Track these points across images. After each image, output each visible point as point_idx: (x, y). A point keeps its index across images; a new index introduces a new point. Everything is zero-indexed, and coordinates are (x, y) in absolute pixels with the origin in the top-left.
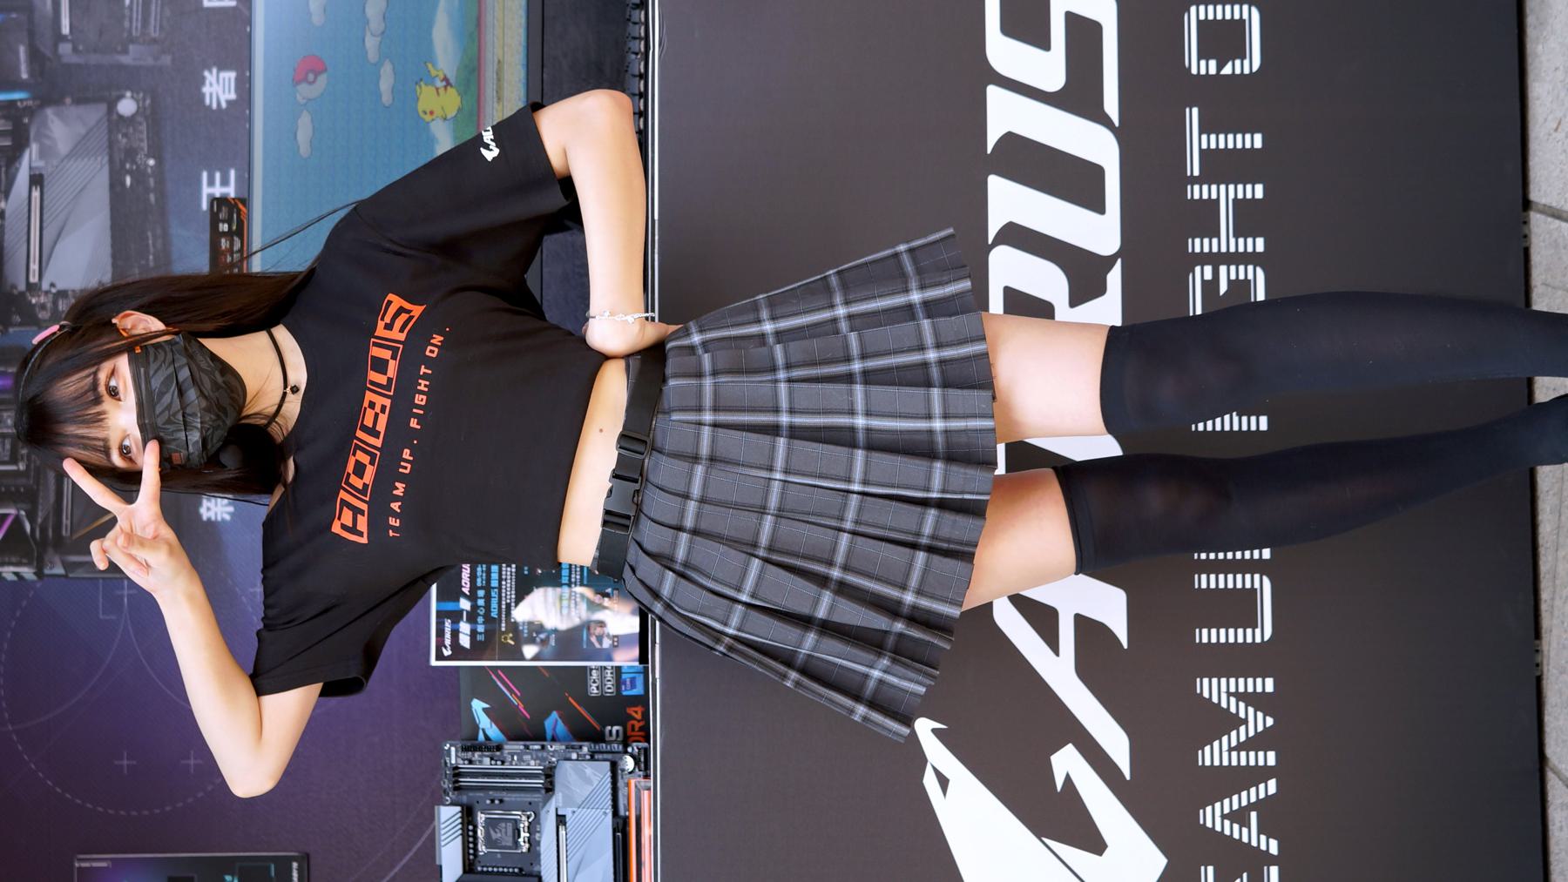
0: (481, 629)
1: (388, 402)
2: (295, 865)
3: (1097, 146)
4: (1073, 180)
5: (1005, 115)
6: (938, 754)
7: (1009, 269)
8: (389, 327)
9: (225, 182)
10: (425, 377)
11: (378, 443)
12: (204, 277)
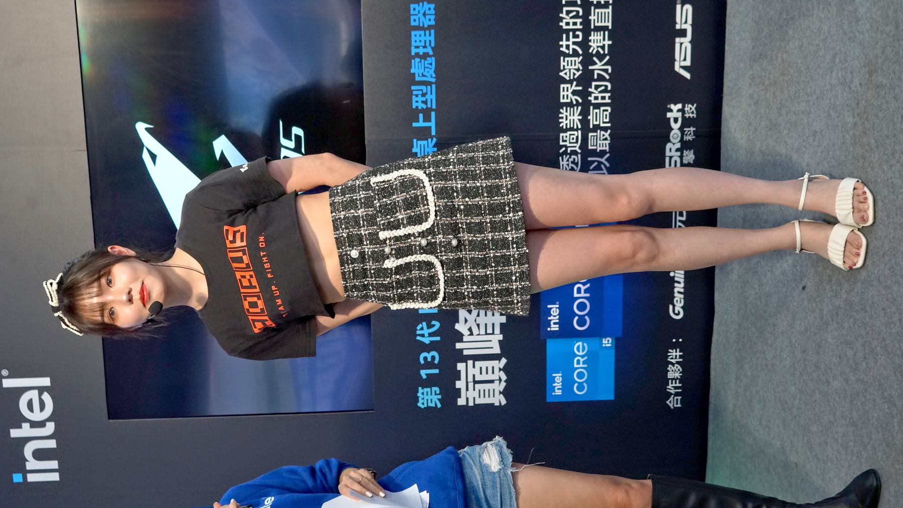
1: (252, 273)
2: (555, 328)
6: (149, 142)
8: (234, 241)
9: (425, 358)
10: (264, 256)
11: (258, 290)
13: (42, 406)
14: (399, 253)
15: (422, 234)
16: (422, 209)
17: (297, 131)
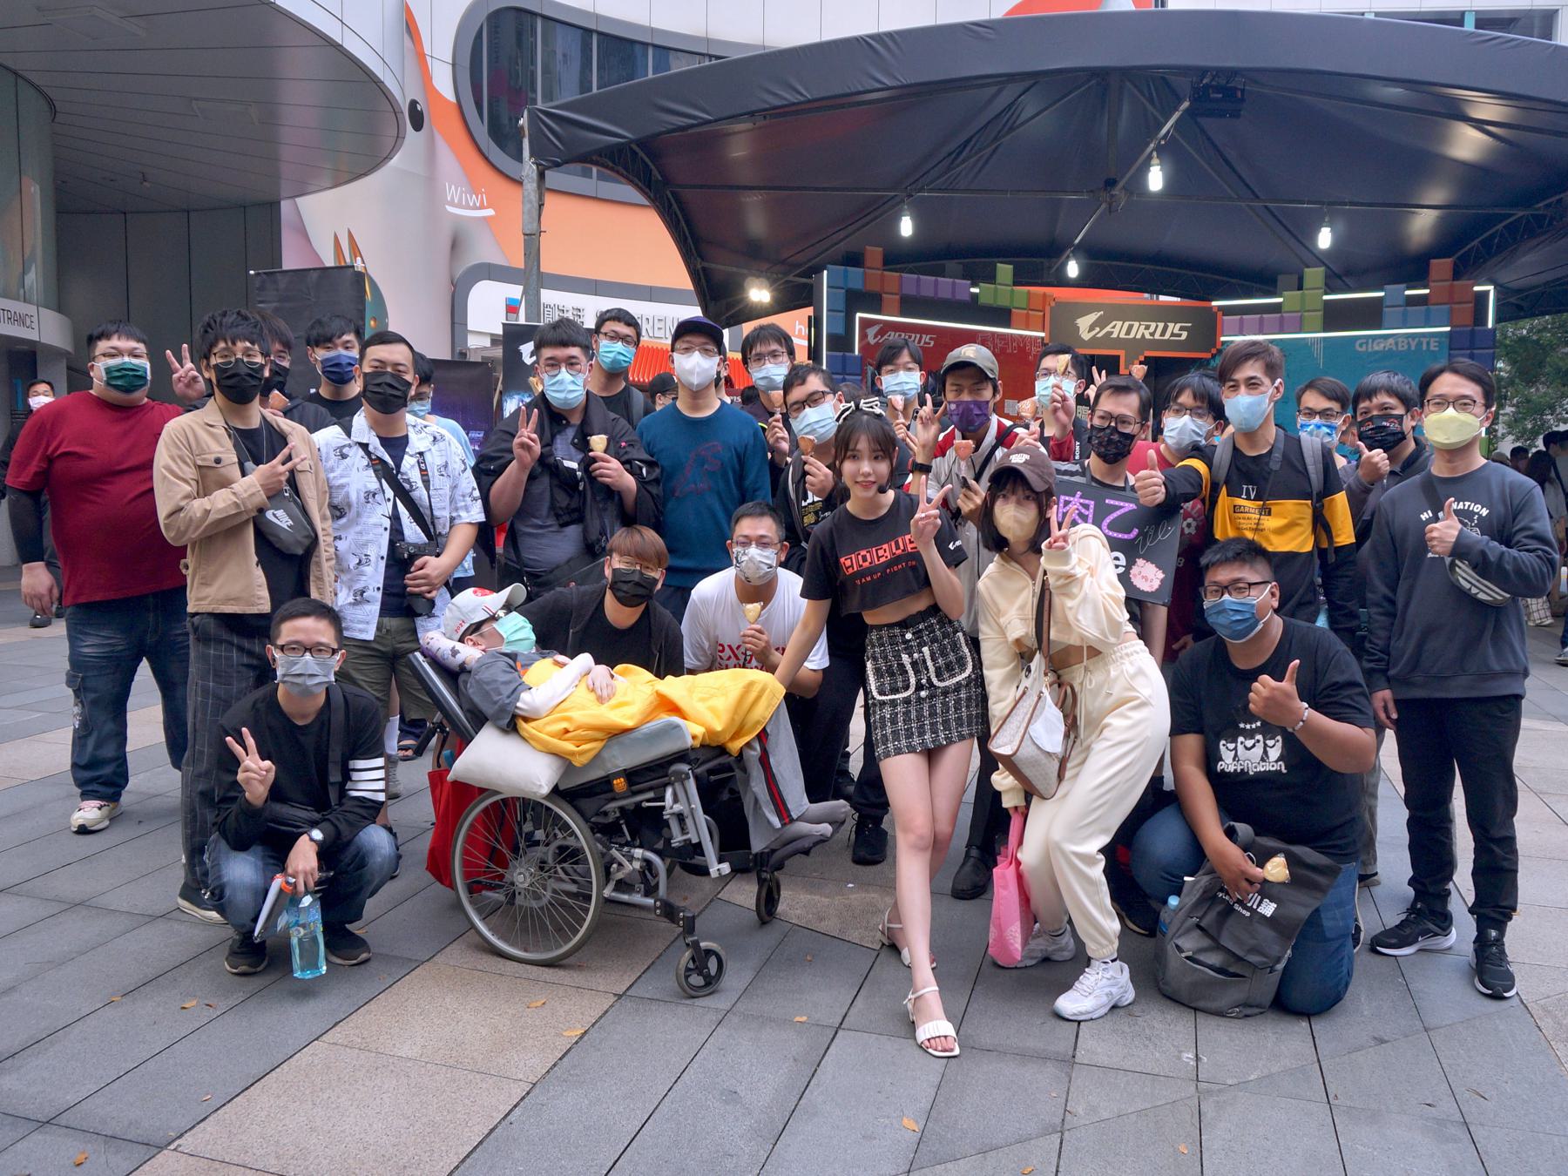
0: (905, 658)
3: (1167, 336)
4: (1163, 334)
5: (1171, 325)
7: (1153, 325)
12: (757, 281)
14: (914, 664)
15: (929, 680)
16: (946, 675)
17: (1185, 335)
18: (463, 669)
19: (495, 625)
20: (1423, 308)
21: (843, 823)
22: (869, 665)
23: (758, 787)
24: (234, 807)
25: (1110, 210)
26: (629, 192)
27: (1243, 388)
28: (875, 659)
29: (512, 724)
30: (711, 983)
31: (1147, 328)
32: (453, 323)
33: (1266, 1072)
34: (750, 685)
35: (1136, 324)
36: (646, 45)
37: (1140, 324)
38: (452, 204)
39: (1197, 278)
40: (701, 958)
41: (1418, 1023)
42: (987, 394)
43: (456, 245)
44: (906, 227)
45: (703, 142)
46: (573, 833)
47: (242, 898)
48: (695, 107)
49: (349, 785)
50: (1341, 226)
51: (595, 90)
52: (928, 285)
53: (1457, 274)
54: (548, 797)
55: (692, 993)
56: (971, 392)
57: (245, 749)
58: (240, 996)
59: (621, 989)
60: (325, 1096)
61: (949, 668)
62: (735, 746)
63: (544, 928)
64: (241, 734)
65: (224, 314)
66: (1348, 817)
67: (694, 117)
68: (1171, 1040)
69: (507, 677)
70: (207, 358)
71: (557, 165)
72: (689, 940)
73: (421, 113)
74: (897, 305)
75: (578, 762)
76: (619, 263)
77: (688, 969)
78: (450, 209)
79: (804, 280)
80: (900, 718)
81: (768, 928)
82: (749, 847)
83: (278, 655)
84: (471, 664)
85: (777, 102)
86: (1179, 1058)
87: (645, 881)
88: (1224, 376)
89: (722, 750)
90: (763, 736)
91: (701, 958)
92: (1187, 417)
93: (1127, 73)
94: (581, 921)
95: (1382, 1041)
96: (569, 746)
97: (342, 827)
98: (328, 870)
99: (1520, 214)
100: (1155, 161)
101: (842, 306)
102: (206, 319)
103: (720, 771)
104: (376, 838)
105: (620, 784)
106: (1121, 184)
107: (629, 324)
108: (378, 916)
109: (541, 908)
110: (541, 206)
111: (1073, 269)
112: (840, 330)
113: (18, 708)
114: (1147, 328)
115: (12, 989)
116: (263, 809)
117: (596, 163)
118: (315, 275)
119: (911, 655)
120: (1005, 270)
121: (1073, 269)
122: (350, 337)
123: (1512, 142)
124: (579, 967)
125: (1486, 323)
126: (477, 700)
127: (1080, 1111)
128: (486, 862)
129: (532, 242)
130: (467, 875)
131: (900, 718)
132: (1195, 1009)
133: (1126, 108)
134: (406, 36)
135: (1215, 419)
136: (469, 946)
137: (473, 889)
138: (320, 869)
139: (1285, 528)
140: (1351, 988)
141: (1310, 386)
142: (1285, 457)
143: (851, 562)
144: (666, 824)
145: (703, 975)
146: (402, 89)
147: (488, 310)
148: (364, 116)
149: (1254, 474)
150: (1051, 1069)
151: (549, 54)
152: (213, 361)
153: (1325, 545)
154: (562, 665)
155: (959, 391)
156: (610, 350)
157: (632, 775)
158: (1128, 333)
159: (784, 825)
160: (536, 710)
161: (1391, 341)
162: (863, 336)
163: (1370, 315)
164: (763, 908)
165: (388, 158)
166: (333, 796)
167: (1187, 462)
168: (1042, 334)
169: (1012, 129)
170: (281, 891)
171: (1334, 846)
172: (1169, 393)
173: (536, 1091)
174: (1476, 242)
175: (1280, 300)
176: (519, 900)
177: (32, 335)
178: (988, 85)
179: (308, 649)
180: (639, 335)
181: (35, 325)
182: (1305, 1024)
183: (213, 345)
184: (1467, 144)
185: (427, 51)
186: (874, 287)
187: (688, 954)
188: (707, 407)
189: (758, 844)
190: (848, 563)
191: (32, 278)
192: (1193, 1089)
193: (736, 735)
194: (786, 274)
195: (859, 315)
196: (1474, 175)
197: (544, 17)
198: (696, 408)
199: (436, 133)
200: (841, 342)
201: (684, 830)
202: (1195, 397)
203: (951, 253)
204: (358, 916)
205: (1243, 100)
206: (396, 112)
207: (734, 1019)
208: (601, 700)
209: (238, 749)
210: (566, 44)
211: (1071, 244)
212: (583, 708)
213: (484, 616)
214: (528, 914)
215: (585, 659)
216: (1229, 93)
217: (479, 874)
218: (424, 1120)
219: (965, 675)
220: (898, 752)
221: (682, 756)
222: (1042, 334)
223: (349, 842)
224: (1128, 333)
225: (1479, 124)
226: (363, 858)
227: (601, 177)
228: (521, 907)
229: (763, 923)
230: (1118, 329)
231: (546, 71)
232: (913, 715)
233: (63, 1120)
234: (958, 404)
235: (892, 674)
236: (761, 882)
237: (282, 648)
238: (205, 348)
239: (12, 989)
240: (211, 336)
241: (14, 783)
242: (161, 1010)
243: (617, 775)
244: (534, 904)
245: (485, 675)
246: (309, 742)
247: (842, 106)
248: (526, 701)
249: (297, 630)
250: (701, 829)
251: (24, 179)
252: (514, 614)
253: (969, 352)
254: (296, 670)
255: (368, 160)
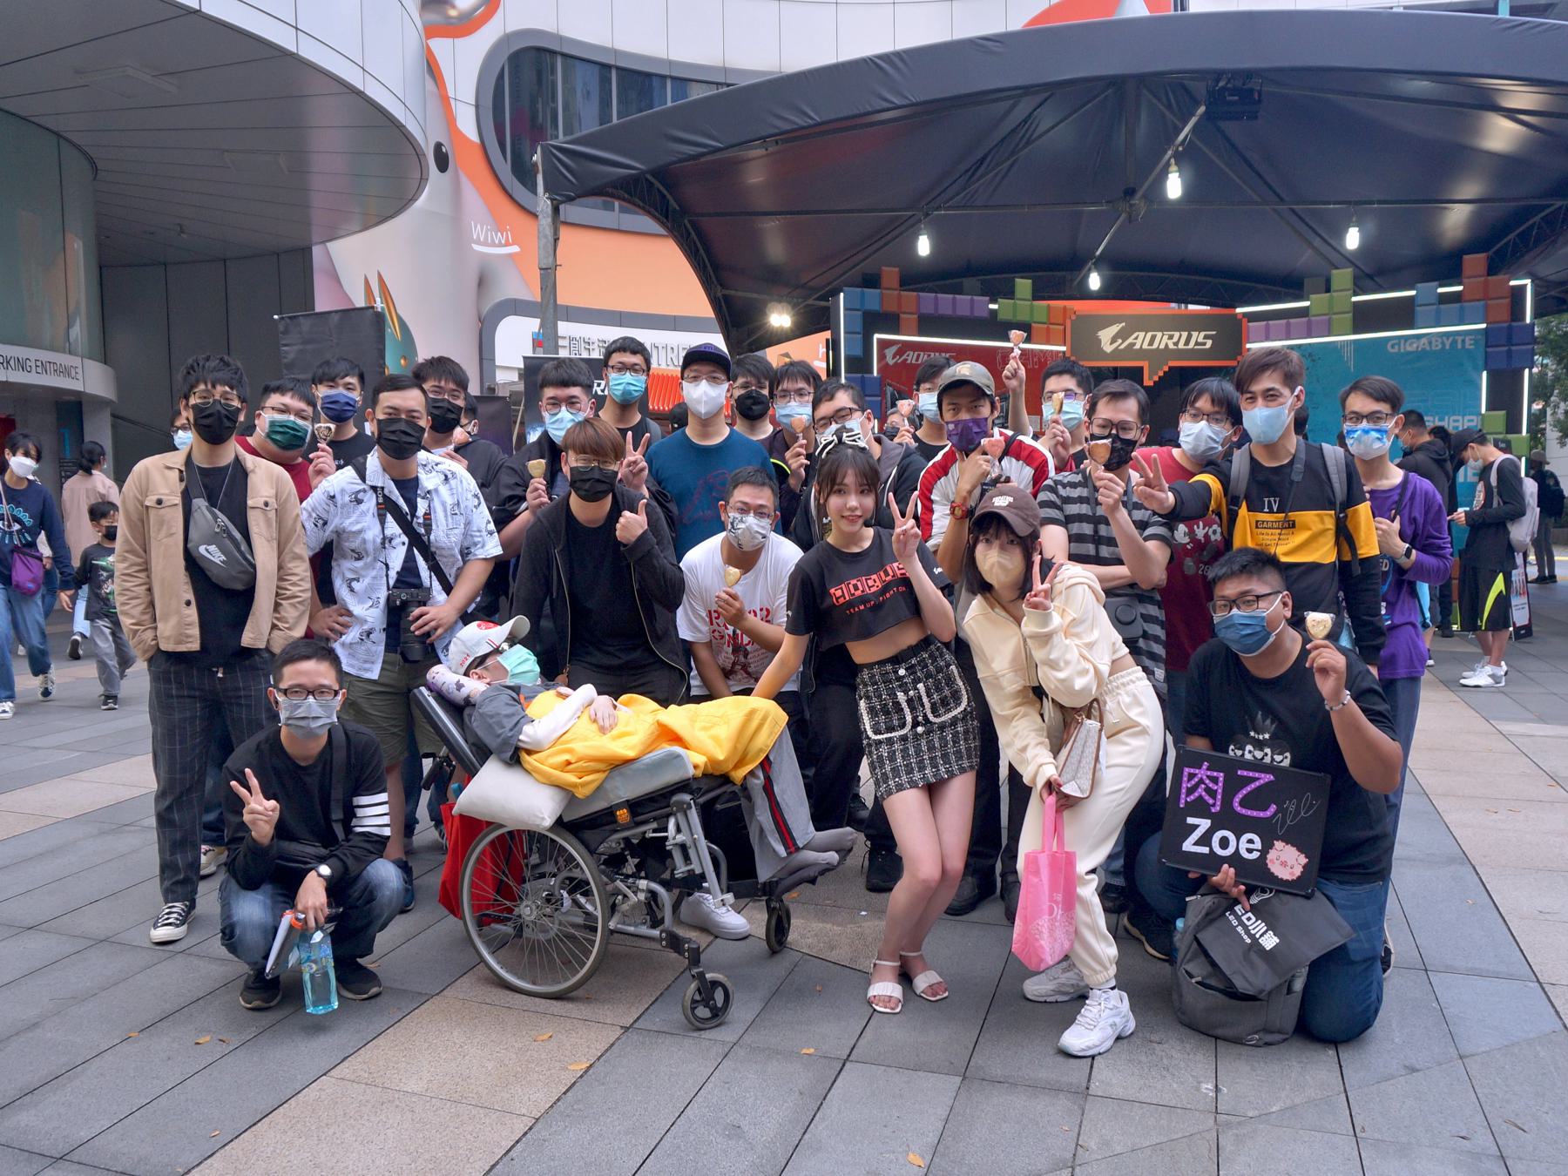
3: (1191, 345)
4: (1187, 343)
5: (1195, 334)
7: (1177, 334)
12: (779, 306)
13: (1250, 851)
14: (910, 701)
15: (925, 716)
16: (942, 711)
17: (1209, 343)
18: (468, 702)
19: (499, 658)
20: (1457, 305)
21: (850, 850)
22: (862, 704)
23: (763, 816)
24: (242, 848)
25: (1130, 219)
26: (646, 222)
27: (1260, 401)
28: (868, 698)
29: (515, 757)
30: (718, 1015)
31: (1171, 337)
32: (481, 359)
33: (1289, 1102)
34: (752, 713)
35: (1159, 334)
36: (664, 77)
37: (1157, 335)
38: (478, 242)
39: (1224, 285)
40: (707, 989)
41: (1452, 1050)
42: (985, 411)
43: (482, 282)
44: (924, 246)
45: (720, 170)
46: (578, 865)
47: (253, 938)
48: (705, 135)
49: (354, 822)
50: (1371, 226)
51: (615, 120)
52: (945, 303)
53: (1492, 270)
54: (551, 829)
55: (699, 1026)
56: (969, 410)
57: (249, 790)
58: (253, 1031)
59: (628, 1021)
60: (331, 1132)
61: (944, 703)
62: (738, 775)
63: (551, 960)
64: (243, 773)
65: (208, 359)
66: (1371, 833)
67: (705, 146)
68: (1188, 1075)
69: (510, 710)
70: (187, 397)
71: (570, 199)
72: (694, 971)
73: (446, 156)
74: (915, 325)
75: (581, 793)
76: (639, 294)
77: (694, 1001)
78: (476, 247)
79: (823, 303)
80: (899, 755)
81: (778, 957)
82: (756, 877)
83: (281, 698)
84: (476, 698)
85: (787, 127)
86: (1198, 1089)
87: (651, 912)
88: (1241, 386)
89: (725, 779)
90: (766, 764)
91: (707, 989)
92: (1203, 423)
93: (1143, 80)
94: (587, 953)
95: (1414, 1070)
96: (571, 778)
97: (350, 862)
98: (338, 906)
99: (1559, 204)
100: (1174, 168)
101: (859, 327)
102: (190, 361)
103: (723, 803)
104: (385, 873)
105: (623, 815)
106: (1140, 194)
107: (634, 352)
108: (390, 945)
109: (549, 941)
110: (556, 240)
111: (1095, 282)
112: (858, 352)
113: (58, 748)
114: (1171, 337)
115: (36, 1025)
116: (270, 846)
117: (618, 198)
118: (336, 317)
119: (906, 692)
120: (1023, 285)
121: (1095, 282)
122: (353, 380)
123: (1550, 135)
124: (587, 1000)
125: (1524, 318)
126: (480, 733)
127: (1093, 1145)
128: (493, 895)
129: (548, 276)
130: (475, 908)
131: (899, 755)
132: (1217, 1038)
133: (1144, 117)
134: (427, 77)
135: (1233, 425)
136: (479, 979)
137: (482, 922)
138: (329, 905)
139: (1308, 541)
140: (1381, 1013)
141: (1355, 387)
142: (1308, 465)
143: (840, 593)
144: (669, 854)
145: (710, 1007)
146: (426, 134)
147: (515, 343)
148: (389, 164)
149: (1274, 487)
150: (1063, 1102)
151: (570, 91)
152: (192, 401)
153: (1347, 557)
154: (565, 697)
155: (956, 410)
156: (619, 383)
157: (635, 806)
158: (1151, 343)
159: (789, 854)
160: (538, 743)
161: (1424, 340)
162: (882, 357)
163: (1402, 314)
164: (773, 938)
165: (413, 199)
166: (339, 830)
167: (1197, 478)
168: (1063, 349)
169: (1028, 143)
170: (291, 928)
171: (1358, 866)
172: (1186, 399)
173: (539, 1125)
174: (1511, 236)
175: (1307, 304)
176: (527, 933)
177: (76, 386)
178: (1002, 99)
179: (311, 692)
180: (648, 362)
181: (80, 376)
182: (1332, 1052)
183: (193, 387)
184: (1501, 135)
185: (451, 94)
186: (891, 307)
187: (693, 986)
188: (718, 433)
189: (764, 873)
190: (839, 593)
191: (77, 331)
192: (1211, 1122)
193: (740, 764)
194: (806, 298)
195: (876, 336)
196: (1507, 166)
197: (564, 55)
198: (705, 435)
199: (464, 179)
200: (859, 364)
201: (687, 859)
202: (1213, 401)
203: (970, 270)
204: (368, 950)
205: (1260, 101)
206: (419, 155)
207: (740, 1052)
208: (603, 730)
209: (242, 791)
210: (586, 79)
211: (1092, 256)
212: (586, 739)
213: (488, 649)
214: (536, 948)
215: (588, 690)
216: (1246, 95)
217: (488, 907)
218: (427, 1156)
219: (960, 709)
220: (900, 788)
221: (684, 786)
222: (1063, 349)
223: (359, 876)
224: (1151, 343)
225: (1511, 114)
226: (371, 892)
227: (622, 210)
228: (528, 940)
229: (774, 952)
230: (1141, 340)
231: (565, 108)
232: (912, 751)
233: (75, 1157)
234: (956, 423)
235: (887, 713)
236: (770, 910)
237: (285, 692)
238: (186, 389)
239: (36, 1025)
240: (192, 378)
241: (49, 822)
242: (175, 1045)
243: (620, 806)
244: (542, 937)
245: (487, 709)
246: (312, 782)
247: (854, 127)
248: (528, 734)
249: (300, 673)
250: (703, 856)
251: (69, 236)
252: (518, 647)
253: (966, 370)
254: (300, 713)
255: (399, 202)
